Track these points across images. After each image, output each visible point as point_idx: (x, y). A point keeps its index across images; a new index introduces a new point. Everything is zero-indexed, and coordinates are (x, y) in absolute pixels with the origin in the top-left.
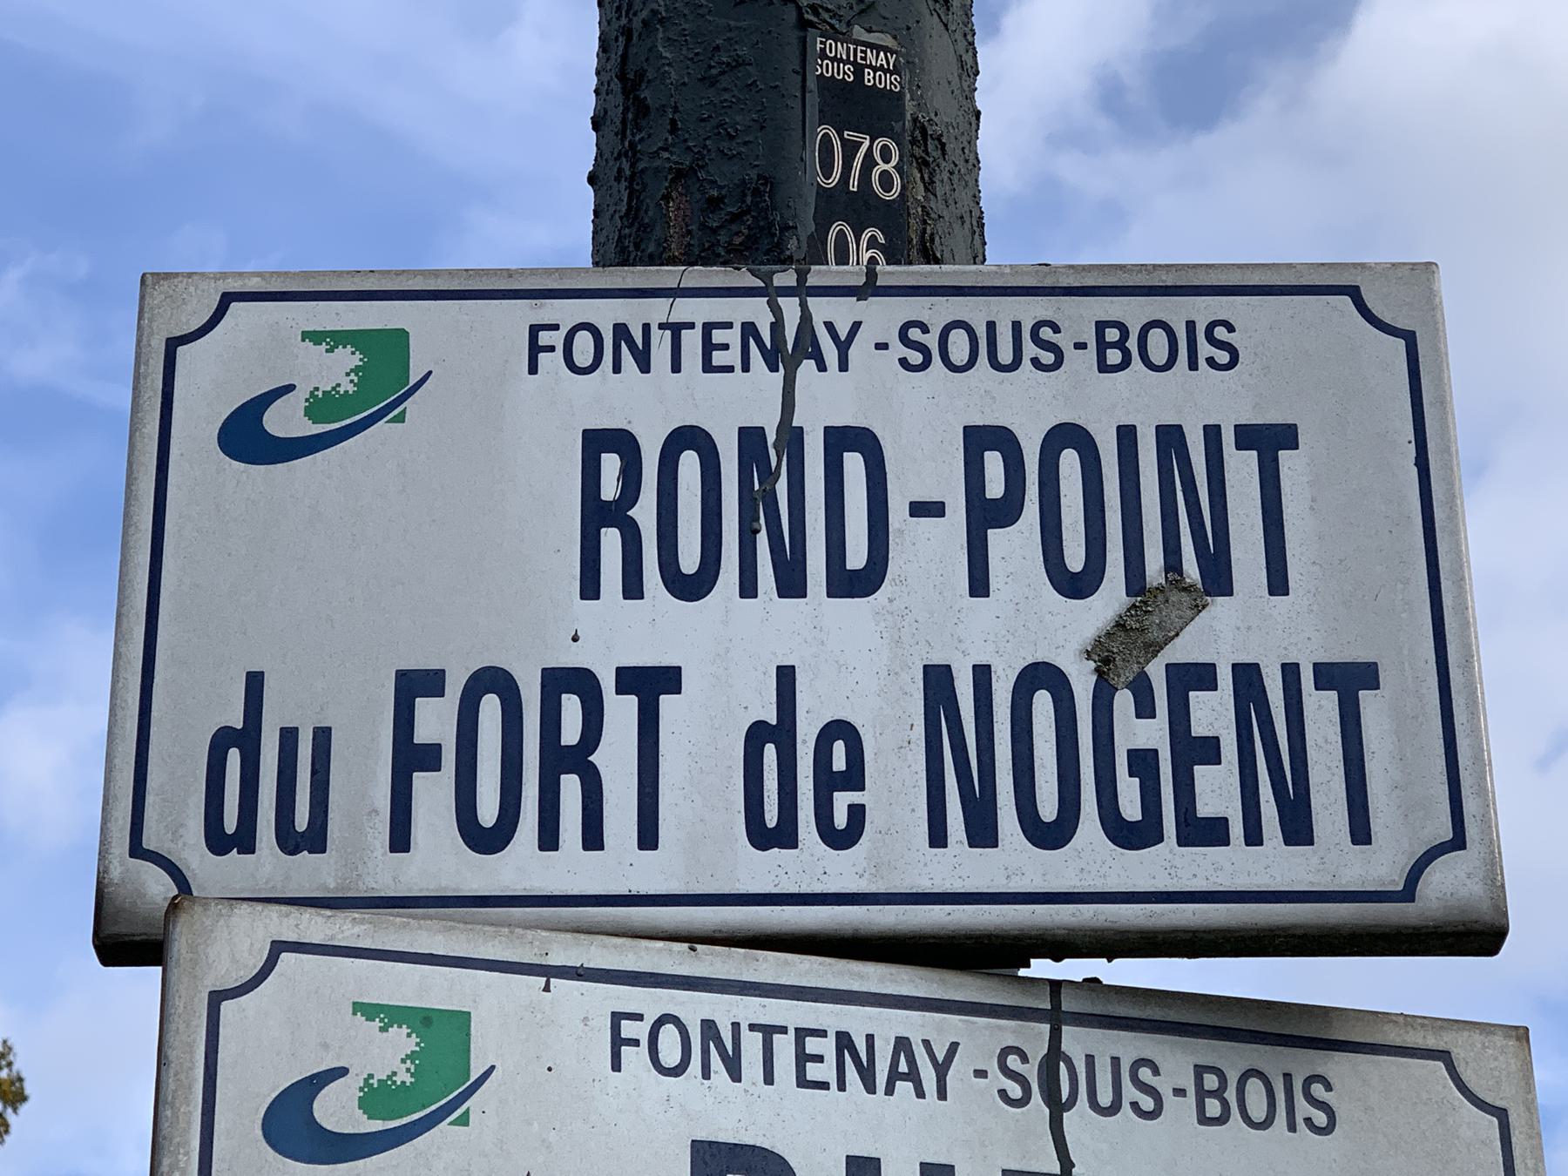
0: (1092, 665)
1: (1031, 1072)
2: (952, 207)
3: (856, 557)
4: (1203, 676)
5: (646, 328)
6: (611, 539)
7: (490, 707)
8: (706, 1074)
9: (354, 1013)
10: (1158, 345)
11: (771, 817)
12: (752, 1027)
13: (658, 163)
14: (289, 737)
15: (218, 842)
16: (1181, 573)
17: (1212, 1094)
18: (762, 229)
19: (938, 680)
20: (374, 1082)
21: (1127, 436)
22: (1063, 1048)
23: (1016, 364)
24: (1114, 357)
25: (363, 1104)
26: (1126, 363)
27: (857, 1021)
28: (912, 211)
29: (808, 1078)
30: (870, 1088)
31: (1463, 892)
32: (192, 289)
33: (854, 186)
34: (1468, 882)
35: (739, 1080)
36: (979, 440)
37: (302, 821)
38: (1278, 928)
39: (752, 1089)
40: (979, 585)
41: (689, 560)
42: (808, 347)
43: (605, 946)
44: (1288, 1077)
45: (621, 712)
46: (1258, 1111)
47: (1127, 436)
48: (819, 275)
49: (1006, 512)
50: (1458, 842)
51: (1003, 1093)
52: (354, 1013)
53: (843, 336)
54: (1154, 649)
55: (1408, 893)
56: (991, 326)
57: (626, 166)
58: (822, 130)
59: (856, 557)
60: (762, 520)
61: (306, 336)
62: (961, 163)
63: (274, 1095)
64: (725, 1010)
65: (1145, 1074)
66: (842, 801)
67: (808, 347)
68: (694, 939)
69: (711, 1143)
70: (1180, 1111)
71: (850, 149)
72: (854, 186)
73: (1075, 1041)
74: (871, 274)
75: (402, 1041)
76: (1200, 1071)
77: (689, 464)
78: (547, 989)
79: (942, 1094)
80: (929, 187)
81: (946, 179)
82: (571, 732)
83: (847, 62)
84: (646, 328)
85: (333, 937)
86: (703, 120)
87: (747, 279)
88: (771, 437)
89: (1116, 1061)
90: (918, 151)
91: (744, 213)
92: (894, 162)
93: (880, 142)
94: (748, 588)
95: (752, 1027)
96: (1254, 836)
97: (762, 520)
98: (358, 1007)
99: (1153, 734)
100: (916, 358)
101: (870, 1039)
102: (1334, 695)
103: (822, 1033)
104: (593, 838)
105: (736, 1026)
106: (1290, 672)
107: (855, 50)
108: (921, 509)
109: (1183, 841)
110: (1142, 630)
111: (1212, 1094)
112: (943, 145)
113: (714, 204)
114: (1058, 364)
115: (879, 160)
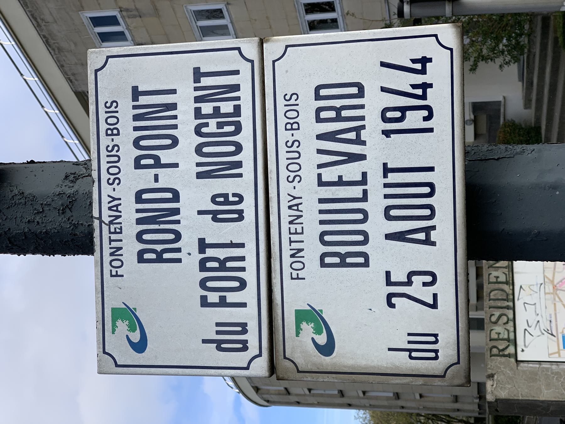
3: (169, 195)
6: (166, 256)
7: (210, 284)
9: (299, 336)
11: (236, 216)
12: (110, 244)
14: (218, 333)
15: (245, 348)
19: (200, 175)
20: (314, 332)
21: (136, 129)
24: (115, 132)
25: (134, 332)
27: (285, 220)
36: (138, 165)
37: (239, 329)
40: (176, 165)
45: (210, 252)
47: (136, 129)
49: (157, 159)
52: (115, 334)
53: (111, 199)
59: (169, 195)
66: (231, 199)
75: (119, 323)
79: (120, 199)
82: (216, 265)
95: (110, 244)
96: (238, 98)
99: (213, 123)
100: (117, 181)
101: (110, 216)
104: (242, 259)
105: (111, 248)
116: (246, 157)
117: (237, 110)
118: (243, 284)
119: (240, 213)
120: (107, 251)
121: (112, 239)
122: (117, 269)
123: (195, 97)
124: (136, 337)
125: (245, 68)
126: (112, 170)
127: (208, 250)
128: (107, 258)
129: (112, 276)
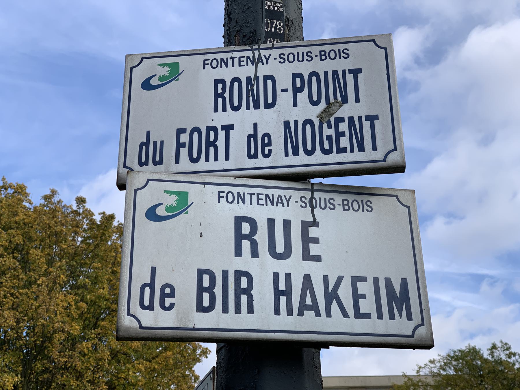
0: (318, 119)
1: (307, 201)
2: (295, 35)
3: (270, 101)
4: (342, 120)
5: (227, 59)
6: (220, 100)
7: (196, 135)
8: (238, 203)
9: (164, 192)
10: (332, 55)
11: (252, 153)
12: (248, 194)
13: (233, 30)
14: (155, 143)
15: (141, 164)
16: (337, 100)
17: (346, 205)
18: (254, 40)
19: (287, 124)
21: (326, 73)
22: (314, 196)
24: (323, 57)
25: (166, 210)
26: (326, 58)
27: (270, 192)
28: (286, 35)
30: (273, 205)
31: (396, 159)
32: (136, 57)
33: (273, 31)
34: (397, 157)
35: (245, 204)
36: (295, 76)
37: (158, 159)
38: (357, 169)
39: (247, 206)
40: (295, 104)
41: (236, 103)
42: (260, 60)
43: (217, 178)
44: (362, 201)
45: (222, 134)
47: (326, 73)
48: (262, 46)
49: (301, 90)
50: (395, 149)
51: (301, 206)
52: (164, 192)
53: (267, 57)
54: (332, 115)
55: (384, 160)
56: (298, 53)
57: (228, 32)
59: (270, 101)
60: (251, 95)
61: (158, 65)
62: (298, 27)
63: (148, 209)
64: (242, 190)
65: (332, 201)
66: (267, 149)
67: (260, 60)
68: (235, 177)
69: (239, 216)
70: (339, 208)
71: (272, 23)
72: (273, 31)
73: (316, 195)
74: (273, 45)
75: (174, 198)
76: (343, 200)
77: (236, 85)
78: (204, 187)
80: (289, 30)
81: (293, 29)
82: (212, 139)
83: (272, 6)
84: (227, 59)
85: (160, 178)
86: (242, 20)
87: (248, 47)
88: (253, 78)
89: (325, 199)
90: (287, 23)
91: (250, 37)
92: (282, 25)
93: (278, 22)
94: (248, 108)
95: (248, 194)
96: (352, 151)
97: (251, 95)
98: (165, 191)
99: (331, 132)
100: (282, 61)
101: (273, 195)
102: (369, 122)
103: (262, 194)
104: (216, 159)
105: (244, 193)
106: (360, 118)
107: (273, 3)
108: (283, 90)
109: (338, 152)
110: (329, 111)
111: (346, 205)
112: (293, 22)
114: (311, 60)
115: (278, 25)
116: (303, 158)
117: (341, 150)
118: (194, 161)
119: (255, 156)
120: (224, 56)
121: (252, 195)
122: (210, 64)
123: (353, 117)
124: (161, 211)
125: (379, 155)
126: (291, 57)
127: (224, 132)
128: (219, 56)
129: (219, 192)
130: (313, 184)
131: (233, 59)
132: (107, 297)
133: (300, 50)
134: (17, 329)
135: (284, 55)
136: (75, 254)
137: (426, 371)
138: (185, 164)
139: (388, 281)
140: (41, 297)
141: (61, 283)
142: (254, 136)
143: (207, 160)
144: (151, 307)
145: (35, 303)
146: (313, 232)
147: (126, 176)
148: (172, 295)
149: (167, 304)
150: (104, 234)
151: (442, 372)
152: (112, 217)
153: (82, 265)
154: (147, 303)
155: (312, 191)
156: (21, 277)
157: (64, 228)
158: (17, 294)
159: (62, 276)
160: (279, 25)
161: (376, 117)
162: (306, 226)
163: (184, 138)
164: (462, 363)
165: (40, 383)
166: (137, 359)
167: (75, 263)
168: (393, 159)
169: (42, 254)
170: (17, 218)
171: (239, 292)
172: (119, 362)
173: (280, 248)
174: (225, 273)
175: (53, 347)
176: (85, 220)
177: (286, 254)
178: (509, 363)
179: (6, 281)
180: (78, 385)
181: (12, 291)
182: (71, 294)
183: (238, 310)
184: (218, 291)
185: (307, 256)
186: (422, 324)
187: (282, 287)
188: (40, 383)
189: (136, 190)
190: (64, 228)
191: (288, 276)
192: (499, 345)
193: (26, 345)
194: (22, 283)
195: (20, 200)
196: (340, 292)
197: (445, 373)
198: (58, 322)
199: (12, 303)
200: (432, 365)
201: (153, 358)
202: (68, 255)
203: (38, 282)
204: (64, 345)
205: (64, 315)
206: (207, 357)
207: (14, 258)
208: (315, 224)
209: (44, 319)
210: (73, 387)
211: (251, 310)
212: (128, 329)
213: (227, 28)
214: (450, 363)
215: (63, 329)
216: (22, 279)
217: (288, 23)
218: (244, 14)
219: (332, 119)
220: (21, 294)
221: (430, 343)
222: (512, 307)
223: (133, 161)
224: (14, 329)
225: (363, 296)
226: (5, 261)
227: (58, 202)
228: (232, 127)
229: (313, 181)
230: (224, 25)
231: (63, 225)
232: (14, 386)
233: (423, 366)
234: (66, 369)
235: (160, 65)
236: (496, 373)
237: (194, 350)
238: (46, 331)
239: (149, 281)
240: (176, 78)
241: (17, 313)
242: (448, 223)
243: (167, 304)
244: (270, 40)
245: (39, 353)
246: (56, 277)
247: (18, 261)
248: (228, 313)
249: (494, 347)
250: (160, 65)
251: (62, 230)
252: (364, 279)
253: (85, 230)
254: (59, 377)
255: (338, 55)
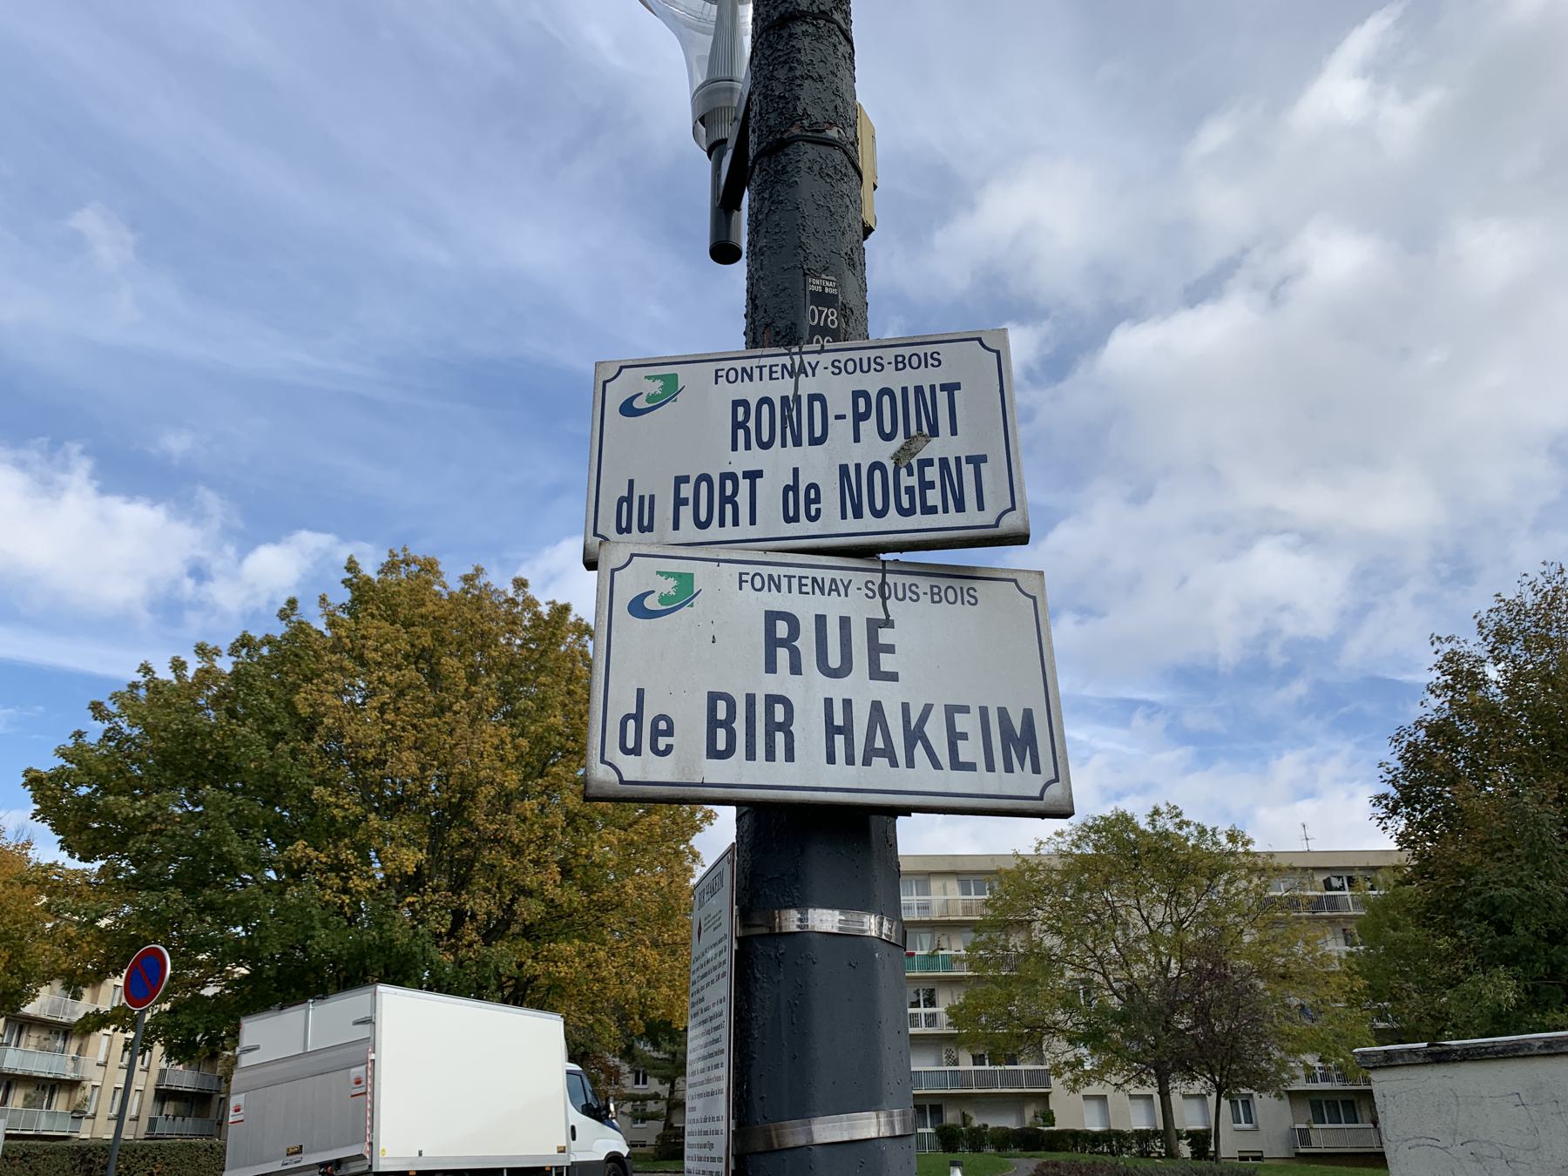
1: (876, 588)
3: (818, 433)
4: (930, 462)
6: (741, 433)
7: (704, 485)
8: (770, 591)
14: (642, 498)
15: (620, 530)
19: (844, 470)
21: (905, 390)
23: (869, 370)
24: (901, 366)
27: (819, 574)
29: (682, 485)
30: (823, 594)
33: (822, 324)
36: (856, 395)
37: (646, 523)
40: (857, 439)
41: (765, 438)
42: (803, 370)
44: (962, 588)
45: (744, 485)
46: (951, 599)
47: (905, 390)
49: (866, 416)
50: (1013, 508)
51: (867, 595)
55: (997, 525)
56: (861, 359)
58: (812, 307)
59: (818, 433)
65: (914, 588)
66: (813, 507)
67: (803, 370)
71: (821, 313)
72: (822, 324)
73: (890, 578)
74: (823, 346)
75: (672, 582)
76: (932, 587)
79: (846, 595)
80: (847, 323)
82: (729, 492)
88: (791, 398)
89: (904, 584)
94: (784, 445)
96: (946, 511)
98: (658, 573)
99: (913, 481)
100: (837, 371)
101: (823, 579)
104: (736, 523)
105: (779, 576)
106: (958, 459)
108: (842, 417)
113: (778, 333)
116: (869, 522)
119: (796, 519)
120: (747, 364)
124: (651, 603)
125: (987, 517)
126: (850, 364)
128: (738, 365)
129: (741, 574)
130: (884, 562)
131: (761, 368)
132: (561, 728)
133: (865, 354)
134: (420, 780)
135: (839, 362)
136: (511, 664)
137: (1047, 849)
138: (688, 531)
139: (1003, 712)
140: (459, 731)
141: (490, 709)
142: (794, 488)
143: (722, 524)
144: (636, 751)
145: (449, 740)
146: (885, 636)
147: (597, 550)
148: (669, 732)
149: (662, 747)
150: (554, 634)
151: (1075, 850)
152: (566, 609)
153: (522, 682)
154: (630, 744)
155: (884, 572)
156: (427, 699)
157: (493, 625)
158: (423, 726)
159: (491, 699)
160: (832, 316)
161: (984, 459)
162: (874, 626)
163: (687, 491)
164: (1106, 837)
165: (456, 862)
166: (605, 826)
167: (510, 678)
168: (1010, 523)
169: (460, 665)
170: (423, 610)
171: (772, 727)
172: (577, 830)
173: (834, 661)
174: (750, 700)
175: (477, 808)
176: (525, 614)
177: (844, 671)
178: (1180, 837)
179: (406, 705)
180: (514, 866)
181: (415, 721)
182: (504, 725)
183: (770, 756)
184: (740, 726)
185: (876, 673)
186: (1057, 780)
187: (839, 720)
188: (456, 862)
189: (613, 571)
190: (493, 625)
191: (847, 703)
192: (1164, 809)
193: (435, 804)
194: (430, 710)
195: (428, 582)
196: (928, 729)
197: (1079, 852)
198: (485, 768)
199: (414, 739)
200: (1060, 840)
201: (630, 825)
202: (500, 667)
203: (454, 708)
204: (493, 805)
205: (494, 757)
206: (712, 824)
207: (418, 670)
208: (888, 623)
209: (463, 764)
210: (507, 869)
211: (790, 756)
212: (601, 785)
213: (750, 319)
214: (1087, 837)
215: (494, 779)
216: (429, 702)
217: (845, 312)
218: (777, 299)
219: (914, 462)
220: (428, 726)
221: (1069, 809)
222: (1180, 752)
223: (608, 526)
224: (417, 779)
225: (964, 736)
226: (403, 676)
227: (486, 585)
228: (759, 474)
229: (883, 557)
230: (746, 316)
231: (492, 620)
232: (416, 867)
233: (1045, 840)
234: (497, 841)
235: (648, 378)
236: (1159, 852)
237: (693, 814)
238: (467, 782)
239: (634, 711)
240: (673, 398)
241: (422, 755)
242: (1080, 622)
243: (662, 745)
244: (818, 340)
245: (454, 817)
246: (483, 700)
247: (424, 675)
248: (755, 760)
249: (1156, 812)
250: (648, 378)
251: (491, 629)
252: (965, 709)
253: (525, 629)
254: (486, 853)
255: (924, 361)
